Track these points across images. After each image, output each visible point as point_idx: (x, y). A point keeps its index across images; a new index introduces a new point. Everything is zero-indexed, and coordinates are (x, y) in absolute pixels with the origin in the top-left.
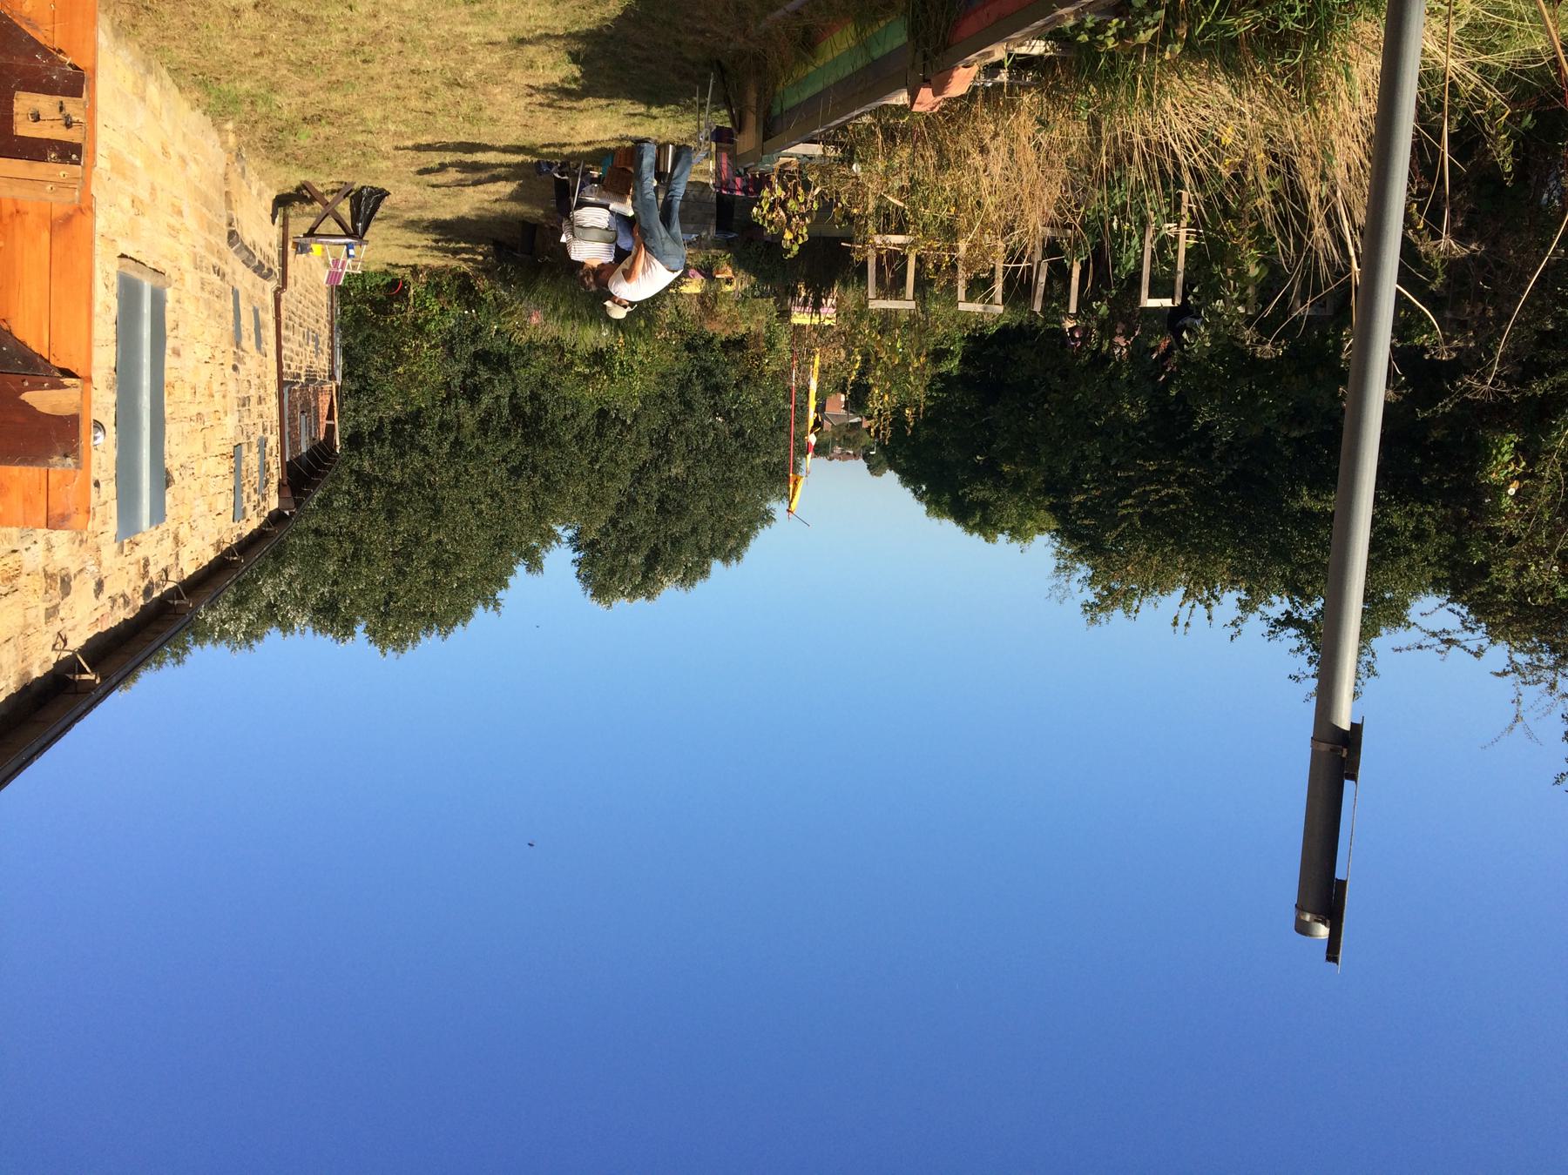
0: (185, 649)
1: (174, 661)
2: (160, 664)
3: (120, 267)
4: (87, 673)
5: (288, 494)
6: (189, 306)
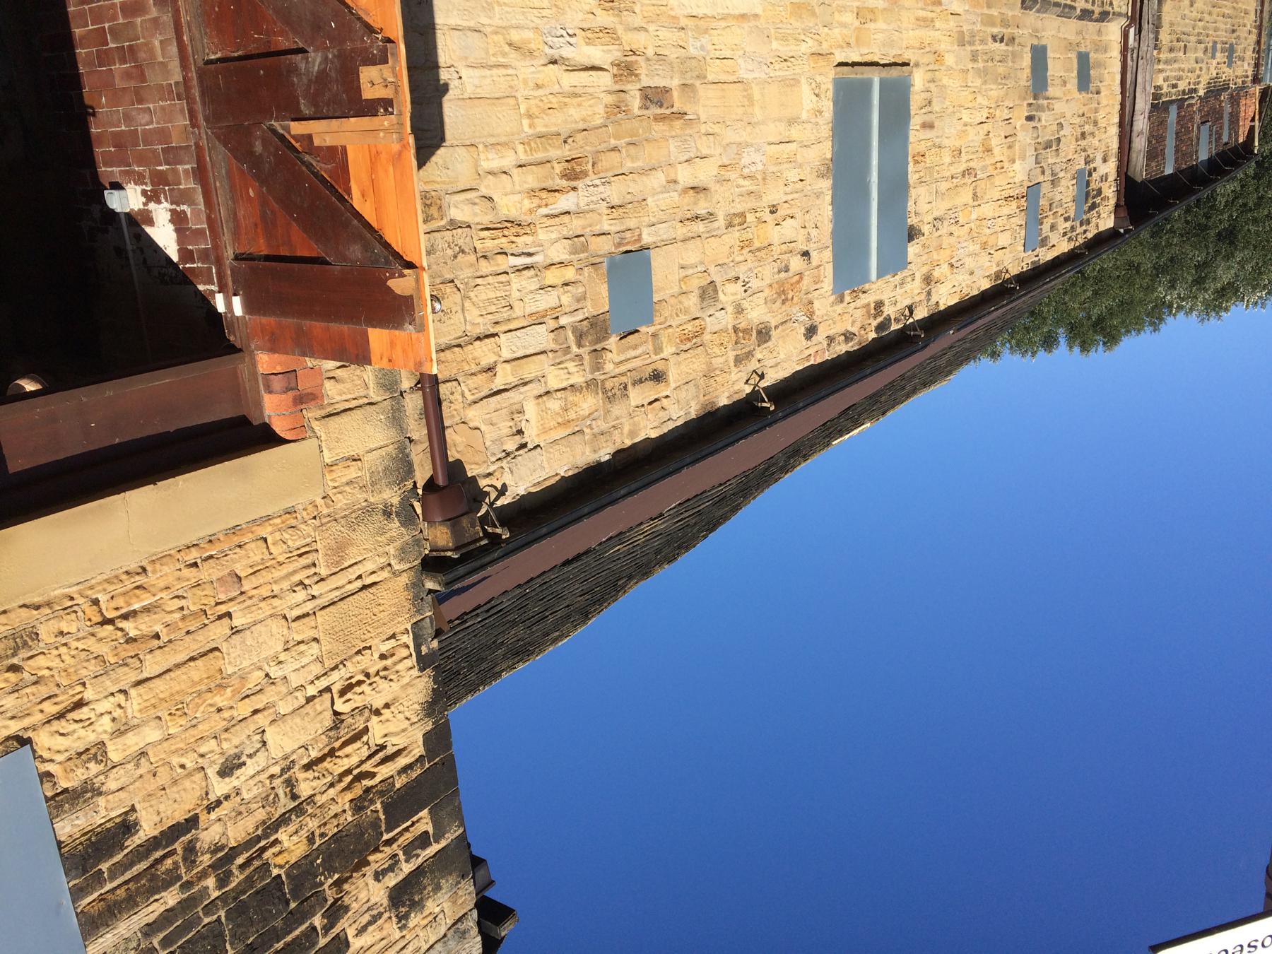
0: (1161, 320)
1: (1151, 328)
2: (1139, 331)
3: (836, 74)
4: (765, 402)
5: (1123, 213)
6: (951, 83)
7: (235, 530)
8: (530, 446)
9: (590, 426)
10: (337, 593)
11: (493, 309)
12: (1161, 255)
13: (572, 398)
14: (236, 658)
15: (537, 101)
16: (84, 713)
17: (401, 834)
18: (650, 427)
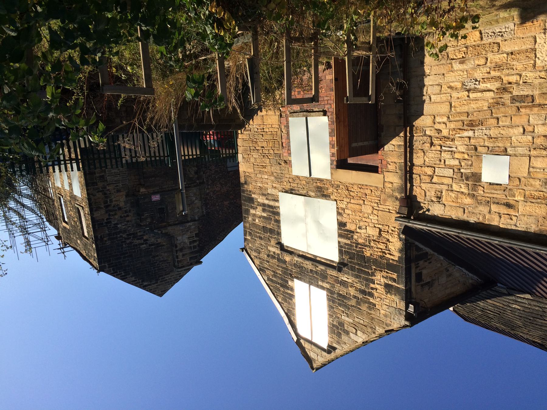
7: (366, 185)
8: (441, 203)
9: (467, 208)
10: (382, 209)
11: (433, 160)
12: (116, 73)
13: (460, 195)
14: (363, 208)
15: (458, 103)
16: (343, 202)
17: (390, 273)
18: (495, 221)
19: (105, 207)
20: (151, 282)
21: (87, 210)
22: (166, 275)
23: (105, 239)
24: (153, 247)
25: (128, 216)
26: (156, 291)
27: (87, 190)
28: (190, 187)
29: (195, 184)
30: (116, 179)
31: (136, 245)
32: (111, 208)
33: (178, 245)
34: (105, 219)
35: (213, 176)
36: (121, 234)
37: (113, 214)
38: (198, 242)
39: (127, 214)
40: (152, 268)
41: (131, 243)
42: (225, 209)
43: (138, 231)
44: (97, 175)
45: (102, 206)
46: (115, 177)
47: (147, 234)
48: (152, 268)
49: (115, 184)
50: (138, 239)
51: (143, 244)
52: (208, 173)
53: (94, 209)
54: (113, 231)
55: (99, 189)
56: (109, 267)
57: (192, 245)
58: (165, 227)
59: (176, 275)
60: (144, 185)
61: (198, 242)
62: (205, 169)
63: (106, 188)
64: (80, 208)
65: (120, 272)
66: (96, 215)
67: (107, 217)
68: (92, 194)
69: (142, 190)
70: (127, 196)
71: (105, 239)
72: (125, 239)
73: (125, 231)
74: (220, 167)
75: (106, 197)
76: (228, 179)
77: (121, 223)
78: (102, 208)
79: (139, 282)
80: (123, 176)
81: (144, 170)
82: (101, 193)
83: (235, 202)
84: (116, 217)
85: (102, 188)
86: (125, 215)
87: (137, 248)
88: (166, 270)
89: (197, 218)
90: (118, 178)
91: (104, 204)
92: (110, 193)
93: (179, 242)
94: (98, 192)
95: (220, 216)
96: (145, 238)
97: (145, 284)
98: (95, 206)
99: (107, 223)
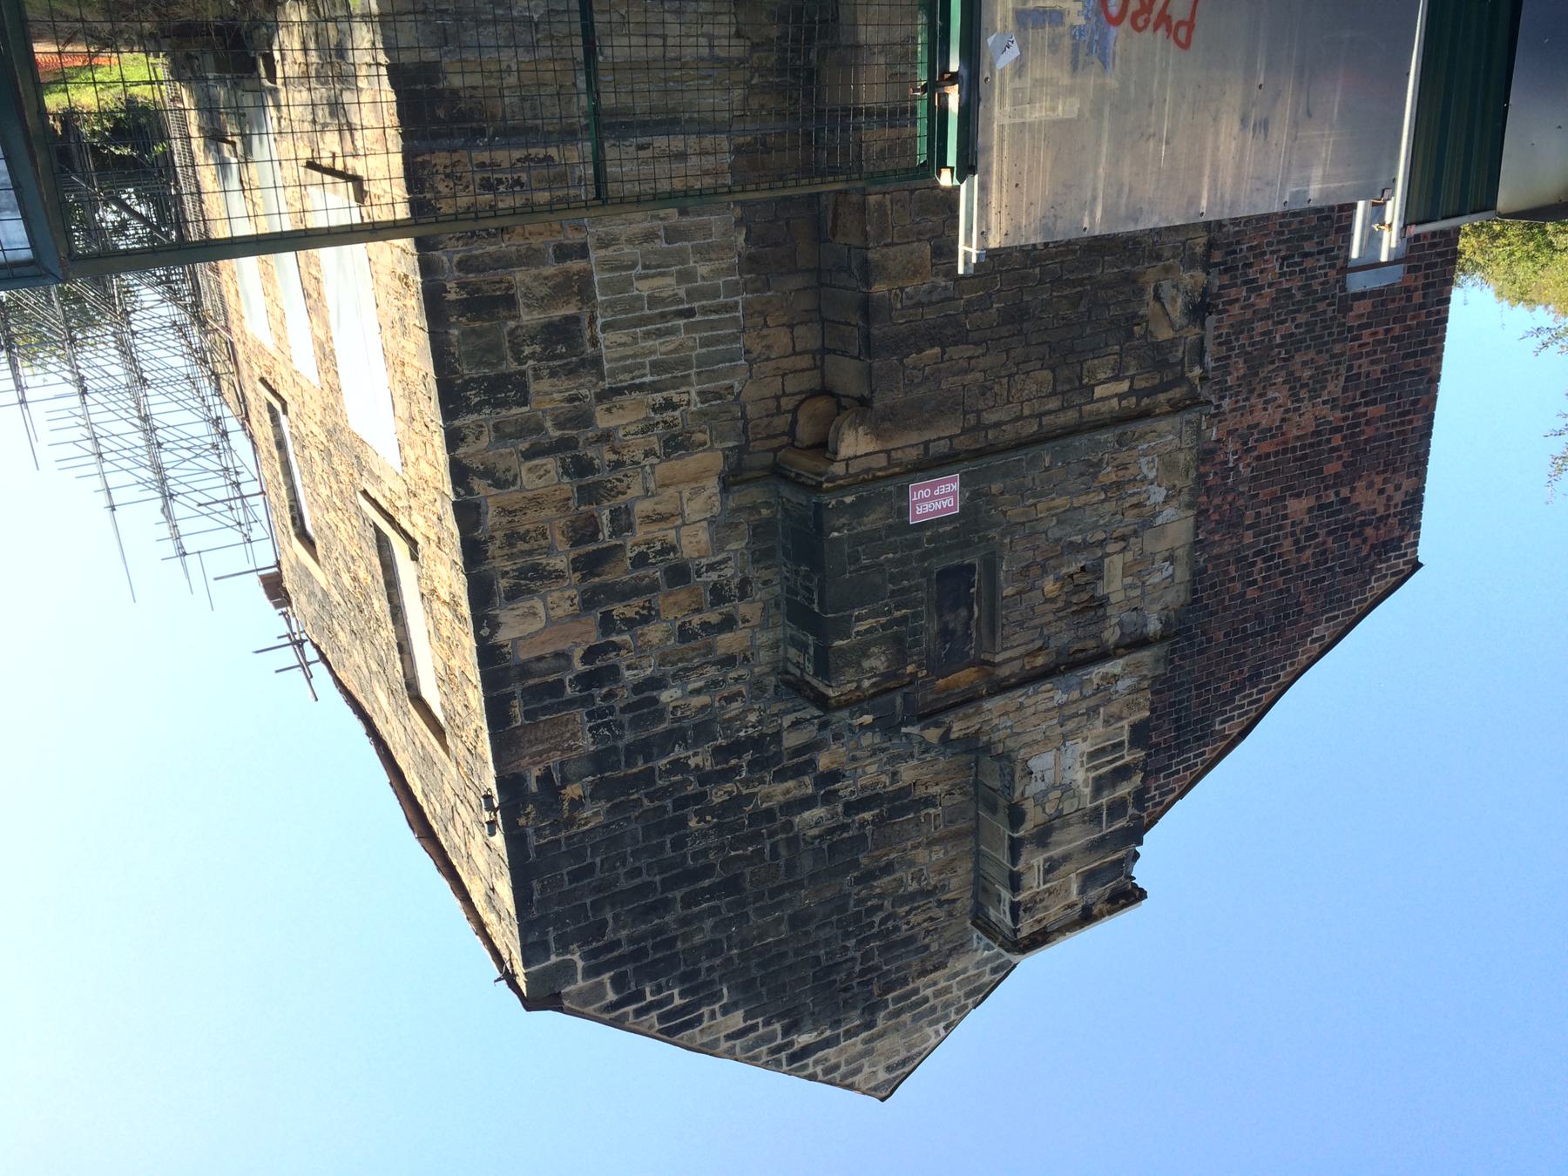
19: (576, 564)
20: (836, 1023)
21: (450, 579)
22: (924, 973)
23: (574, 791)
24: (867, 816)
25: (728, 623)
26: (858, 1070)
27: (453, 439)
28: (1145, 415)
29: (1176, 393)
30: (661, 348)
31: (769, 814)
32: (618, 573)
33: (1029, 805)
34: (578, 653)
35: (1259, 327)
36: (679, 752)
37: (630, 613)
38: (1137, 779)
39: (726, 608)
40: (851, 943)
41: (736, 802)
42: (1287, 545)
43: (787, 721)
44: (530, 317)
45: (560, 562)
46: (659, 334)
47: (837, 737)
48: (851, 943)
49: (654, 387)
50: (781, 776)
51: (807, 803)
52: (1236, 309)
53: (503, 584)
54: (629, 737)
55: (540, 428)
56: (590, 972)
57: (1104, 800)
58: (970, 699)
59: (979, 965)
60: (864, 402)
61: (1137, 779)
62: (1226, 280)
63: (585, 420)
64: (400, 548)
65: (659, 990)
66: (513, 627)
67: (594, 638)
68: (488, 473)
69: (855, 444)
70: (730, 481)
71: (574, 791)
72: (705, 778)
73: (703, 731)
74: (1309, 262)
75: (589, 494)
76: (1337, 348)
77: (681, 676)
78: (559, 575)
79: (771, 1037)
80: (712, 325)
81: (879, 289)
82: (550, 463)
83: (1346, 500)
84: (654, 633)
85: (559, 425)
86: (713, 617)
87: (771, 834)
88: (927, 947)
89: (1154, 626)
90: (672, 342)
91: (575, 544)
92: (618, 464)
93: (1034, 787)
94: (528, 455)
95: (1251, 593)
96: (824, 761)
97: (804, 1039)
98: (508, 566)
99: (587, 681)
